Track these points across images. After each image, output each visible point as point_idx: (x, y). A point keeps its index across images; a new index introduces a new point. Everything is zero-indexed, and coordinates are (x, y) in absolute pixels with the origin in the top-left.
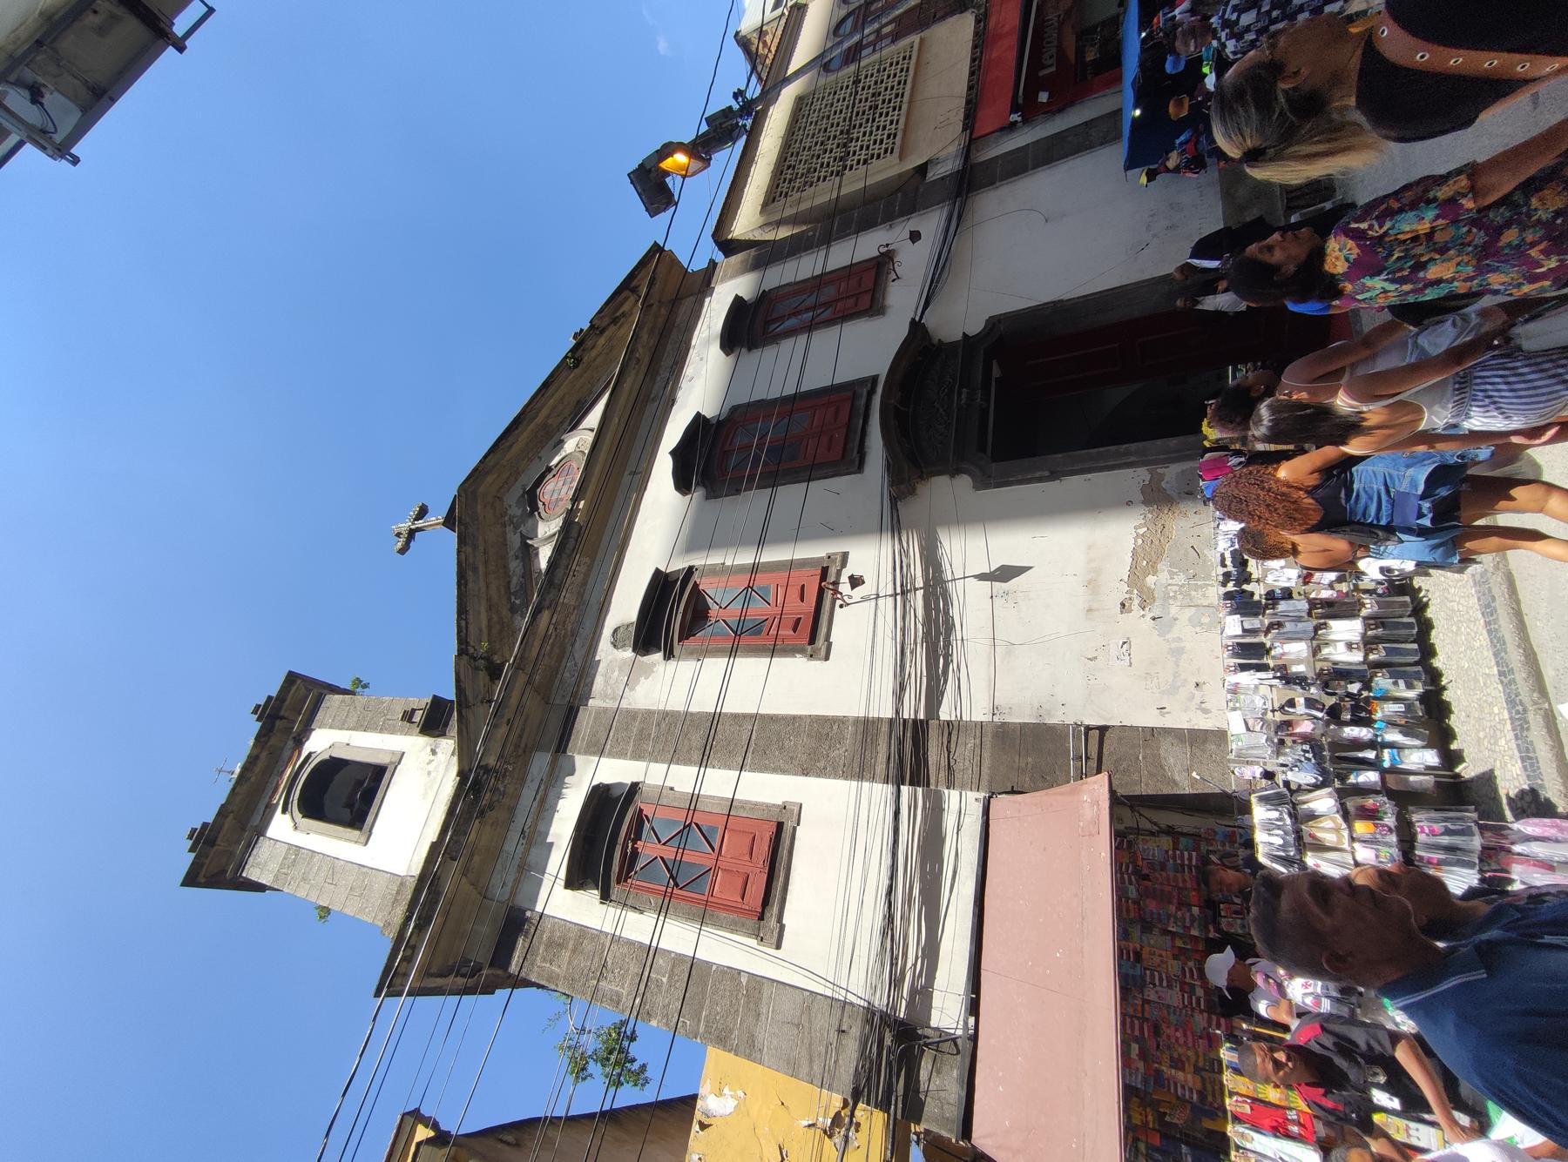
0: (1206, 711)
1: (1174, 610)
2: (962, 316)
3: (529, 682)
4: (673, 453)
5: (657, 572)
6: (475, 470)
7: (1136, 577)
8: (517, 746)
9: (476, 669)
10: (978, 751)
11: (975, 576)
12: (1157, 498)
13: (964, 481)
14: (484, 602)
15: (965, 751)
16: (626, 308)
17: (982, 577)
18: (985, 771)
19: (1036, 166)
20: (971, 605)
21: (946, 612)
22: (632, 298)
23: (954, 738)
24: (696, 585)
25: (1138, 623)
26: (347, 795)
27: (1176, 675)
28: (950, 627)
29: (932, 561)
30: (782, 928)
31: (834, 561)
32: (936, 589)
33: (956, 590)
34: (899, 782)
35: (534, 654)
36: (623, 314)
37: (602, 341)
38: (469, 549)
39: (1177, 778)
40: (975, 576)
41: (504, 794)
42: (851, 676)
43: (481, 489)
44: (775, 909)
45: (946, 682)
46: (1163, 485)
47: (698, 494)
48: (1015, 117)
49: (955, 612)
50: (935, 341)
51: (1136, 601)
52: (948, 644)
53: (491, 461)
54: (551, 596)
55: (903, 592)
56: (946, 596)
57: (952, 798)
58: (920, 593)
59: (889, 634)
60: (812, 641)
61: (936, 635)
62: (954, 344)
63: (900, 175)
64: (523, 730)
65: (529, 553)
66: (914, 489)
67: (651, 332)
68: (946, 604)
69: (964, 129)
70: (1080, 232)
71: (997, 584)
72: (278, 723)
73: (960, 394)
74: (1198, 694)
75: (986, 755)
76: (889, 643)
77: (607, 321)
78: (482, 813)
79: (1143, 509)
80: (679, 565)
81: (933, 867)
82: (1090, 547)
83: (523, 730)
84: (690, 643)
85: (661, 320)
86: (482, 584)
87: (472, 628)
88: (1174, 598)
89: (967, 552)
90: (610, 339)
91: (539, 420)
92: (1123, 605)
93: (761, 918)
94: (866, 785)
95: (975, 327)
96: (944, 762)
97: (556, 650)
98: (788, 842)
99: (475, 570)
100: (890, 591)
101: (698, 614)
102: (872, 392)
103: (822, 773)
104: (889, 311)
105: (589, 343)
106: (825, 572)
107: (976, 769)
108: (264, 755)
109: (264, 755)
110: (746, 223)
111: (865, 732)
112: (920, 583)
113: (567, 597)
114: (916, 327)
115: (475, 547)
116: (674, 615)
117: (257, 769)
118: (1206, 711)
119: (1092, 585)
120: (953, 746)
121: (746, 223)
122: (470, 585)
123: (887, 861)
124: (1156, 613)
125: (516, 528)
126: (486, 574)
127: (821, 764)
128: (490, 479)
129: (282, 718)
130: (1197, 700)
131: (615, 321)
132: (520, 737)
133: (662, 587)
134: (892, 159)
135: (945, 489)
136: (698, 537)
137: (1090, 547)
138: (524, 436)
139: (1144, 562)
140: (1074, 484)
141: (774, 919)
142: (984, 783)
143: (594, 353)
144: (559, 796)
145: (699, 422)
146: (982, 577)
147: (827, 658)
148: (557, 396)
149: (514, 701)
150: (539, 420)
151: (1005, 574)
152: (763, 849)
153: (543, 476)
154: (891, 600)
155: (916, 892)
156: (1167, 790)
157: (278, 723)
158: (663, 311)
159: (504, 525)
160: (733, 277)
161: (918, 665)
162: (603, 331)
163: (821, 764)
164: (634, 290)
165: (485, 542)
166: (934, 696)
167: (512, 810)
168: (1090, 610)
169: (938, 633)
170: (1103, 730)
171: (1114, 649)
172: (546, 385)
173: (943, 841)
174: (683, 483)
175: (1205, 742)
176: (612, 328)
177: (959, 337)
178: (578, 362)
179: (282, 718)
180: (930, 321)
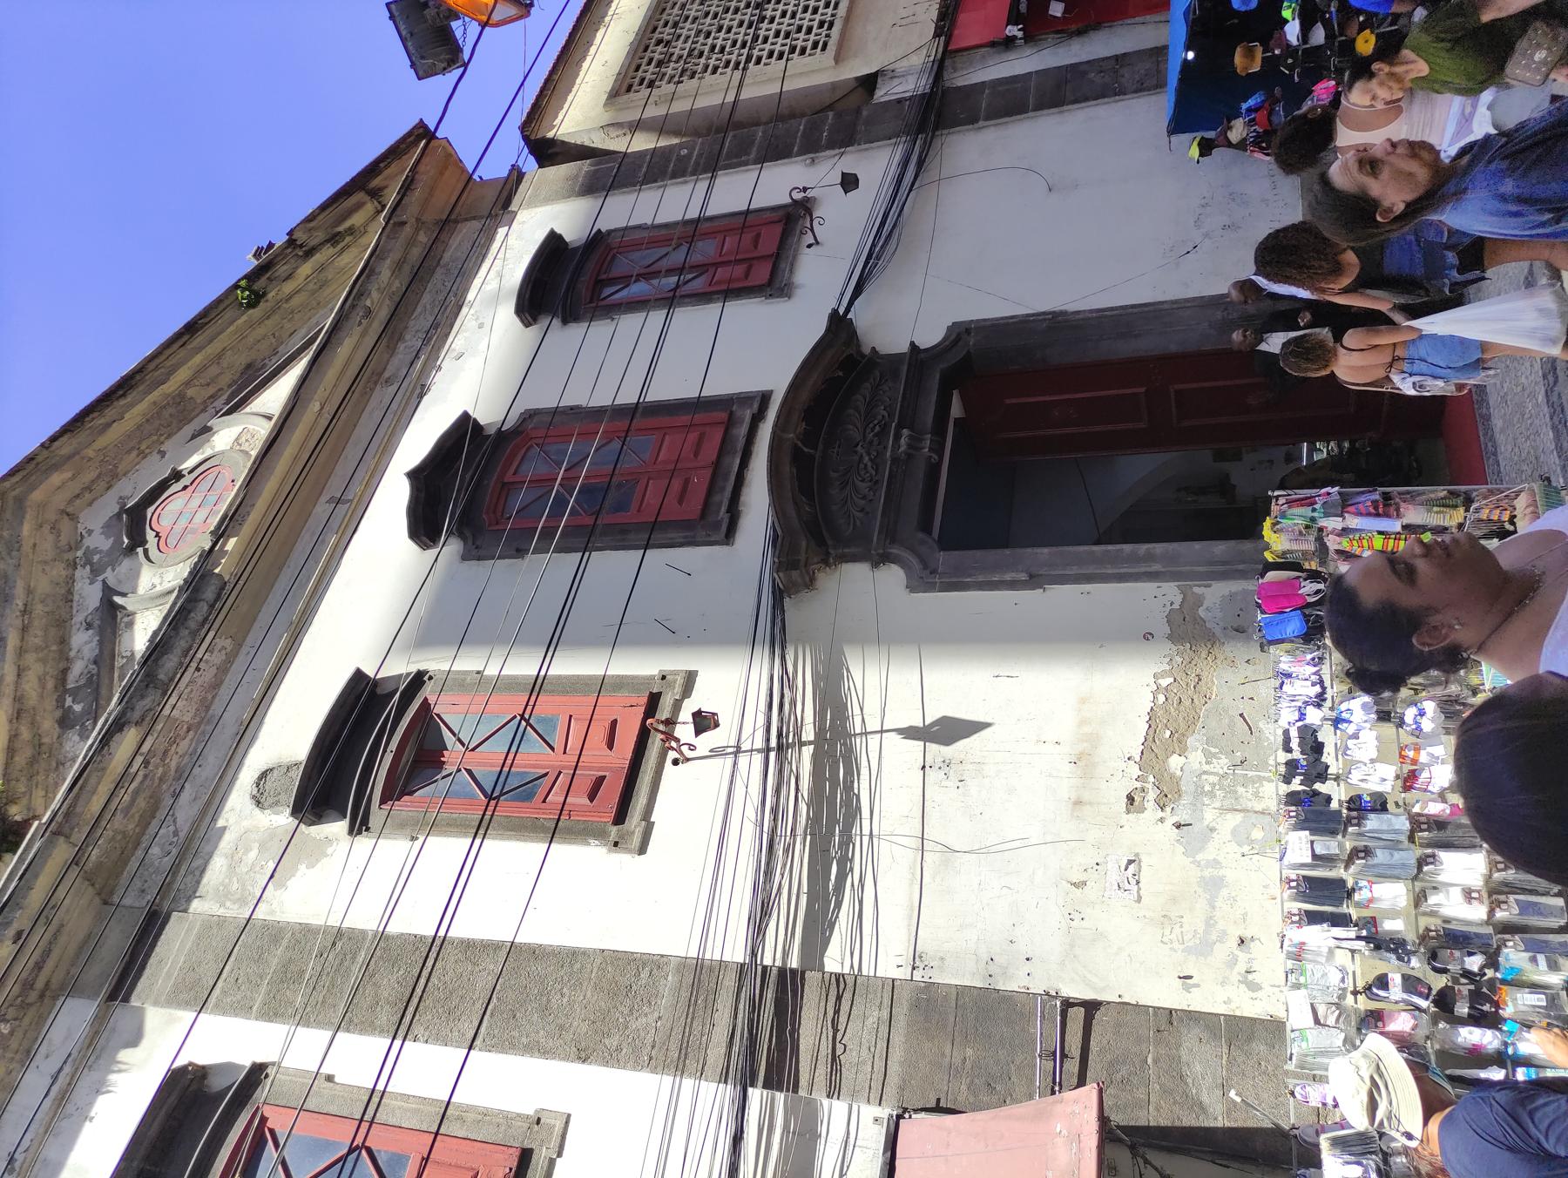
0: (1254, 987)
1: (1209, 815)
2: (906, 319)
3: (75, 861)
4: (413, 475)
5: (359, 675)
6: (30, 459)
7: (1152, 754)
8: (28, 985)
10: (884, 1030)
11: (900, 731)
12: (1189, 632)
13: (893, 576)
16: (357, 220)
17: (910, 733)
18: (894, 1068)
19: (1040, 107)
20: (891, 776)
21: (849, 787)
22: (370, 207)
25: (1150, 831)
27: (1210, 922)
28: (853, 812)
29: (832, 700)
31: (671, 685)
32: (836, 745)
33: (868, 751)
34: (747, 1080)
35: (96, 805)
36: (351, 231)
37: (306, 269)
39: (1205, 1099)
40: (900, 731)
42: (669, 888)
43: (37, 496)
45: (839, 905)
46: (1201, 612)
47: (451, 548)
48: (1013, 30)
49: (863, 788)
50: (866, 350)
51: (1152, 795)
52: (847, 841)
53: (65, 447)
54: (147, 702)
55: (781, 747)
56: (850, 758)
57: (835, 1114)
58: (808, 752)
59: (751, 813)
60: (620, 818)
61: (821, 820)
63: (834, 86)
64: (47, 953)
66: (812, 580)
67: (398, 267)
68: (849, 772)
69: (937, 35)
70: (1093, 216)
71: (933, 748)
73: (897, 437)
74: (1242, 956)
75: (898, 1039)
76: (749, 828)
79: (1169, 648)
80: (400, 667)
82: (1083, 701)
83: (47, 953)
85: (416, 253)
88: (1212, 795)
89: (888, 691)
90: (322, 268)
91: (171, 387)
92: (1131, 799)
95: (930, 335)
96: (825, 1049)
97: (142, 803)
100: (759, 744)
101: (424, 756)
102: (758, 417)
104: (798, 293)
105: (282, 269)
106: (654, 701)
107: (879, 1064)
110: (580, 116)
111: (696, 986)
112: (809, 734)
113: (180, 707)
114: (839, 325)
118: (1254, 987)
119: (1083, 761)
121: (580, 116)
124: (1183, 817)
126: (21, 652)
128: (56, 478)
130: (1241, 967)
131: (334, 239)
132: (39, 966)
133: (362, 702)
134: (825, 59)
135: (864, 587)
136: (440, 622)
137: (1083, 701)
138: (137, 410)
139: (1165, 733)
140: (1063, 597)
143: (288, 287)
144: (99, 1088)
145: (464, 431)
146: (910, 733)
147: (642, 850)
148: (211, 350)
149: (36, 898)
151: (948, 731)
153: (162, 486)
154: (758, 759)
156: (1189, 1120)
158: (423, 238)
159: (73, 565)
160: (548, 200)
161: (796, 871)
162: (309, 253)
164: (375, 194)
165: (29, 591)
168: (1078, 803)
169: (833, 821)
170: (1091, 1007)
171: (1114, 876)
174: (425, 524)
175: (1250, 1039)
177: (904, 348)
180: (863, 317)
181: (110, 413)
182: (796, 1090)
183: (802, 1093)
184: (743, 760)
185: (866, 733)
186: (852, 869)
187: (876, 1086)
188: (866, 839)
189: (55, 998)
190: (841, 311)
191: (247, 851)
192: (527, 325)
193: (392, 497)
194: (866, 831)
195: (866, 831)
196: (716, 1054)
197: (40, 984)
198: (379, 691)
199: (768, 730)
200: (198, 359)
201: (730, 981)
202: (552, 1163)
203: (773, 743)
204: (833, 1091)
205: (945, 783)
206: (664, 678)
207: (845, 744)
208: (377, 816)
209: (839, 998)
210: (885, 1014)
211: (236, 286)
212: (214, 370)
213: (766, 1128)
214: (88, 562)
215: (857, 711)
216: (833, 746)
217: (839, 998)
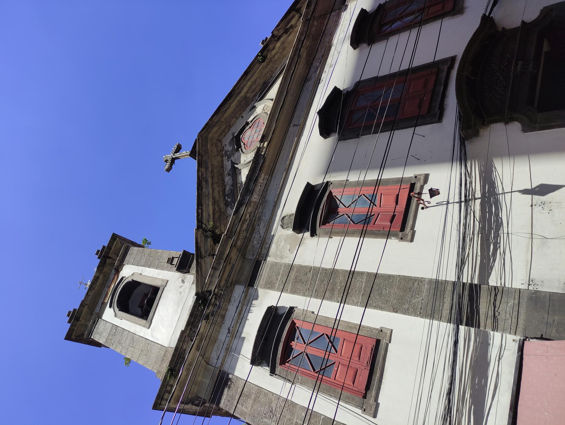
6: (207, 124)
9: (206, 237)
10: (516, 308)
13: (516, 126)
14: (211, 199)
15: (506, 308)
16: (293, 22)
17: (525, 192)
18: (521, 322)
20: (516, 212)
21: (497, 215)
23: (499, 298)
24: (331, 193)
26: (140, 301)
29: (488, 180)
30: (377, 405)
31: (419, 180)
32: (491, 197)
33: (505, 200)
34: (459, 322)
36: (292, 27)
37: (278, 44)
38: (203, 170)
40: (520, 191)
41: (219, 307)
43: (210, 135)
44: (373, 393)
45: (494, 260)
50: (500, 29)
52: (497, 236)
53: (216, 119)
57: (496, 338)
58: (478, 202)
59: (455, 226)
61: (487, 227)
62: (516, 29)
65: (235, 172)
68: (497, 209)
72: (108, 260)
73: (516, 65)
75: (522, 311)
77: (282, 31)
78: (207, 318)
81: (480, 381)
84: (328, 227)
86: (210, 189)
87: (204, 214)
89: (513, 174)
90: (283, 43)
91: (242, 94)
93: (365, 397)
94: (436, 322)
96: (491, 313)
98: (378, 375)
99: (207, 181)
100: (457, 200)
101: (332, 210)
103: (406, 312)
106: (412, 186)
107: (514, 320)
108: (101, 277)
109: (101, 277)
111: (436, 288)
112: (478, 194)
113: (255, 198)
115: (207, 169)
116: (317, 211)
117: (98, 284)
120: (498, 303)
122: (204, 190)
123: (448, 373)
125: (229, 158)
126: (212, 184)
127: (406, 306)
128: (215, 129)
129: (110, 258)
131: (286, 31)
132: (229, 276)
133: (311, 195)
138: (234, 104)
141: (372, 401)
142: (520, 329)
143: (274, 52)
146: (525, 192)
147: (412, 240)
150: (242, 94)
151: (544, 190)
152: (367, 355)
153: (244, 128)
155: (468, 395)
157: (108, 260)
161: (475, 249)
163: (406, 306)
165: (212, 166)
166: (485, 269)
167: (223, 317)
169: (490, 228)
172: (246, 73)
173: (488, 364)
174: (325, 132)
176: (285, 36)
177: (519, 24)
178: (264, 58)
179: (110, 258)
180: (497, 15)
181: (226, 106)
182: (479, 327)
183: (482, 328)
184: (450, 206)
185: (504, 193)
186: (500, 247)
187: (513, 328)
188: (505, 235)
189: (234, 285)
190: (487, 14)
191: (281, 242)
192: (355, 48)
193: (313, 120)
194: (506, 231)
195: (506, 231)
196: (446, 312)
197: (230, 281)
198: (315, 189)
199: (460, 194)
200: (249, 83)
201: (450, 288)
202: (387, 345)
203: (463, 199)
204: (495, 328)
205: (543, 211)
206: (382, 331)
207: (495, 198)
208: (318, 230)
209: (496, 295)
210: (517, 302)
211: (258, 56)
212: (254, 86)
213: (467, 339)
214: (226, 155)
215: (500, 184)
216: (489, 198)
217: (496, 295)
